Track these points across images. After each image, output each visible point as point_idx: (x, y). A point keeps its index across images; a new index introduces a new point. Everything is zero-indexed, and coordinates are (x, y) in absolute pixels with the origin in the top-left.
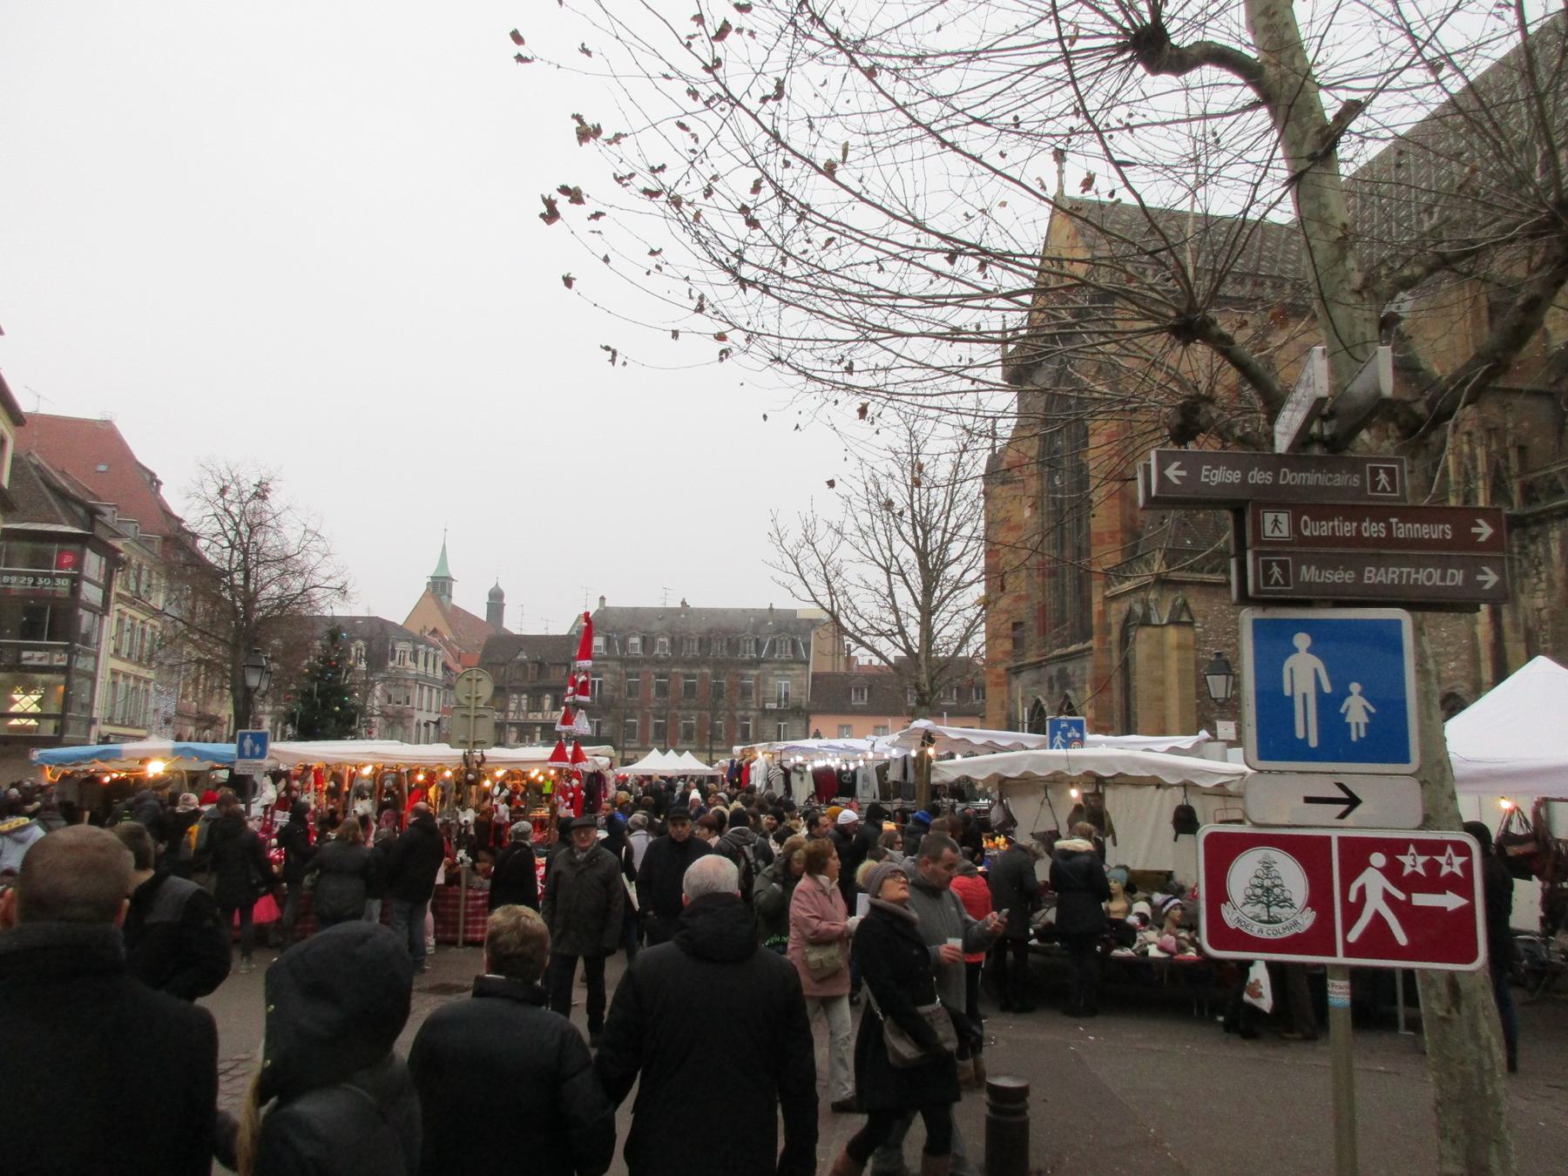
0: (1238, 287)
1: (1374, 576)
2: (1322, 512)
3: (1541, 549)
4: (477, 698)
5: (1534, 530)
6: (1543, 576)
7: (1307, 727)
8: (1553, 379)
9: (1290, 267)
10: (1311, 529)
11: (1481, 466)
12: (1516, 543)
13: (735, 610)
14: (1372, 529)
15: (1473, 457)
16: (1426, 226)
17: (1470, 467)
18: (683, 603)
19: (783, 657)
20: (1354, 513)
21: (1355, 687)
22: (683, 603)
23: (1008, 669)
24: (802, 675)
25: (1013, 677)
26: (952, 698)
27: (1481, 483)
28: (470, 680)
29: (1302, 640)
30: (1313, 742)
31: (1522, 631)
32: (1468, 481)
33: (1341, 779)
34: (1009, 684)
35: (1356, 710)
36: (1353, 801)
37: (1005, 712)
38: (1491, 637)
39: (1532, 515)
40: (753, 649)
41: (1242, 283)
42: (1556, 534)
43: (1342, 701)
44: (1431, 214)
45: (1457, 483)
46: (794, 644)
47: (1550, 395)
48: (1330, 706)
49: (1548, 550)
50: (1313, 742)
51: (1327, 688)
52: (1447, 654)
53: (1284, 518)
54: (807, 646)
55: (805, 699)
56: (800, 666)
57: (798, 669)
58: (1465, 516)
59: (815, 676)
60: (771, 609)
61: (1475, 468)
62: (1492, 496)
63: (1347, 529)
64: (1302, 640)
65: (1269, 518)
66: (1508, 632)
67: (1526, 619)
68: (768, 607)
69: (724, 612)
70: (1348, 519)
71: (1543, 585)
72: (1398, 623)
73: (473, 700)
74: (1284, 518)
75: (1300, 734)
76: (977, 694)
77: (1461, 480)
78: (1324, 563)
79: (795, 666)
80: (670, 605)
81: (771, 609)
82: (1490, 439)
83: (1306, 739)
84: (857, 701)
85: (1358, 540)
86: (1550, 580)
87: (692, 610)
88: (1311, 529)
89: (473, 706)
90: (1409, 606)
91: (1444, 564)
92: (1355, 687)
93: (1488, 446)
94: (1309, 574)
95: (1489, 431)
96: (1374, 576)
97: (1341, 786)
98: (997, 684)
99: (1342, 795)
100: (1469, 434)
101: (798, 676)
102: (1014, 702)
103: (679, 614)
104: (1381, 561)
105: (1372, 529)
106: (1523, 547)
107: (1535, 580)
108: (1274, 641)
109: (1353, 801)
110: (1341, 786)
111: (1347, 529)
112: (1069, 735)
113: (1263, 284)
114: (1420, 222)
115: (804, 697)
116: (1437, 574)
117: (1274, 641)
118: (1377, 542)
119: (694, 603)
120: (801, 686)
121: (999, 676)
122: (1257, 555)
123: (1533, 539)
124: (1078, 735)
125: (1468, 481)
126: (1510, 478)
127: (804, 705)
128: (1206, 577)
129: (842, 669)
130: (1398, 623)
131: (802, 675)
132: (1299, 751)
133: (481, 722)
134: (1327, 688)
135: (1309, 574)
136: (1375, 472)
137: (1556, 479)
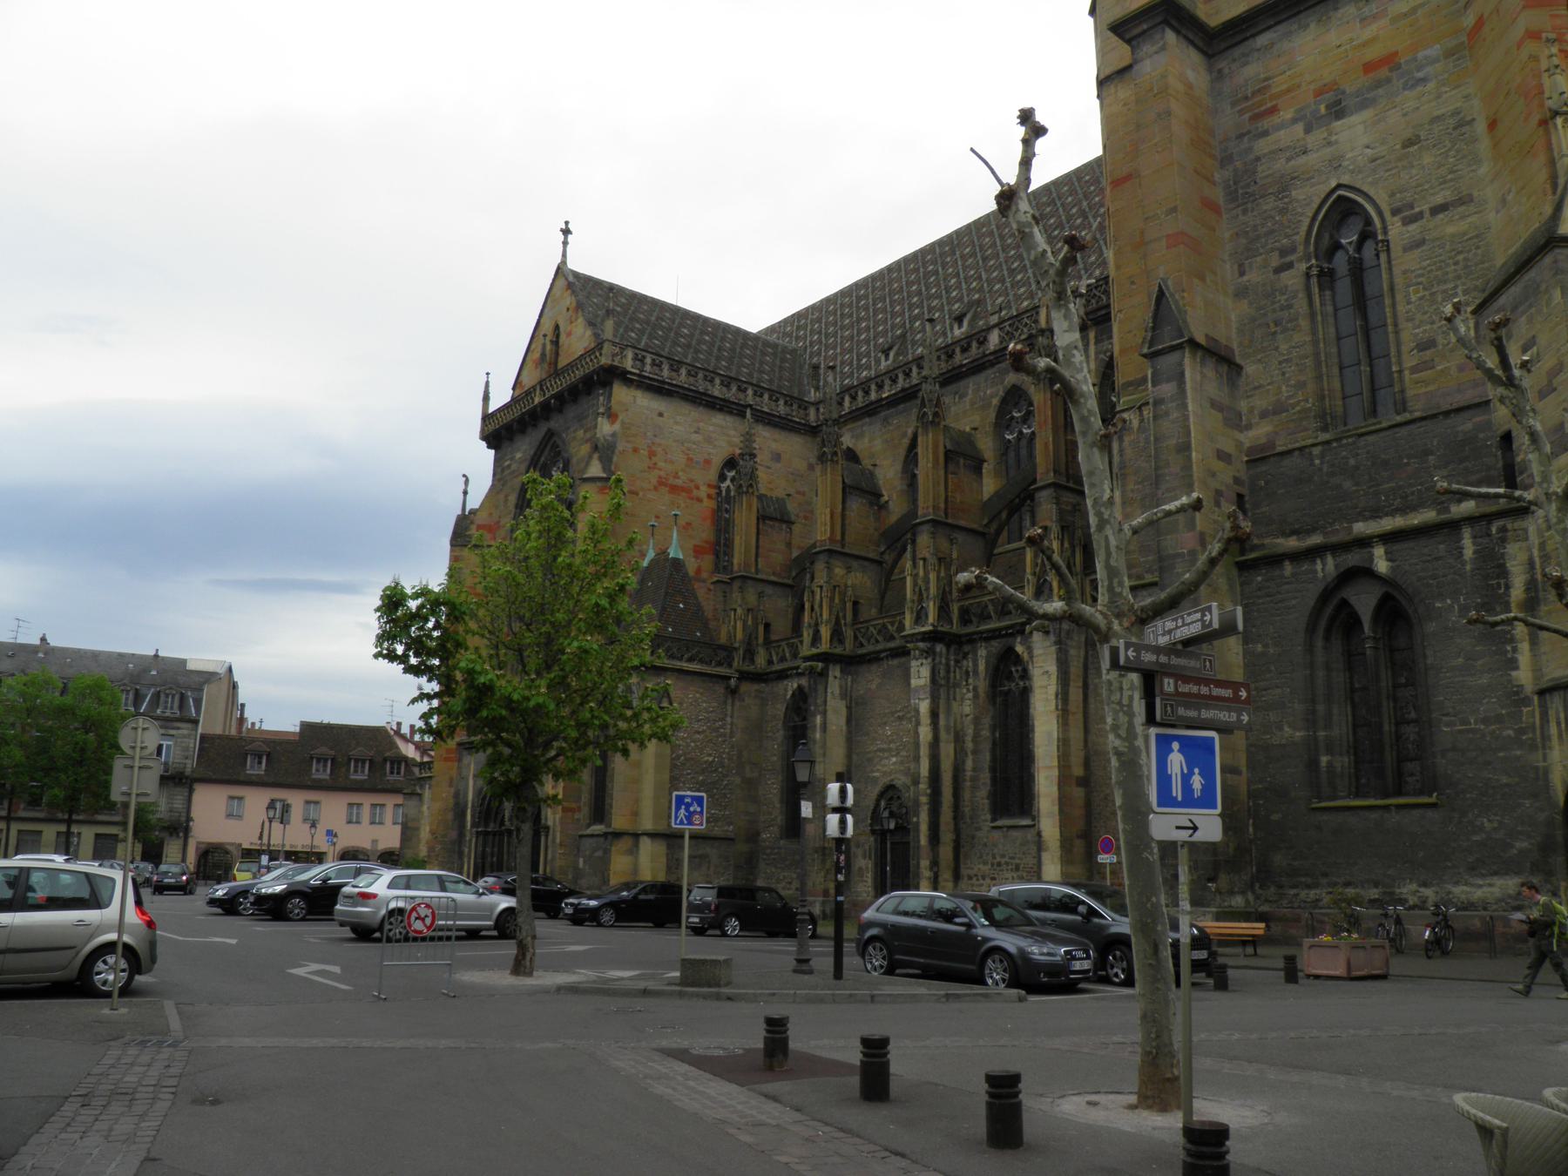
0: (724, 389)
1: (1206, 714)
2: (1187, 680)
3: (970, 664)
4: (142, 748)
5: (966, 648)
6: (971, 687)
7: (1177, 791)
8: (985, 522)
9: (637, 326)
10: (1184, 688)
11: (933, 590)
12: (952, 658)
13: (109, 655)
14: (1204, 690)
15: (927, 581)
16: (884, 365)
17: (923, 588)
18: (43, 639)
19: (168, 714)
20: (1199, 681)
21: (1196, 771)
22: (43, 639)
23: (459, 744)
24: (189, 736)
25: (465, 753)
26: (363, 772)
27: (931, 604)
28: (136, 729)
29: (1176, 746)
30: (1180, 799)
31: (952, 734)
32: (921, 600)
33: (1190, 817)
34: (460, 760)
35: (1197, 782)
36: (1195, 828)
37: (452, 790)
38: (930, 737)
39: (967, 635)
40: (130, 701)
41: (728, 386)
42: (982, 652)
43: (1191, 778)
44: (887, 356)
45: (913, 601)
46: (183, 698)
47: (983, 534)
48: (1186, 779)
49: (976, 665)
50: (1180, 799)
51: (1185, 771)
52: (890, 750)
53: (1171, 681)
54: (198, 703)
55: (190, 766)
56: (189, 725)
57: (185, 729)
58: (1235, 686)
59: (203, 737)
60: (156, 656)
61: (927, 589)
62: (939, 616)
63: (1195, 689)
64: (1176, 746)
65: (1166, 680)
66: (943, 735)
67: (955, 724)
68: (152, 653)
69: (95, 656)
70: (1196, 684)
71: (970, 695)
72: (1213, 739)
73: (138, 750)
74: (1171, 681)
75: (1174, 795)
76: (392, 768)
77: (916, 598)
78: (1187, 706)
79: (179, 725)
80: (22, 640)
81: (156, 656)
82: (940, 565)
83: (1176, 797)
84: (255, 769)
85: (1198, 696)
86: (975, 689)
87: (54, 649)
88: (1184, 688)
89: (137, 757)
90: (1218, 730)
91: (1229, 710)
92: (1196, 771)
93: (939, 572)
94: (1181, 711)
95: (940, 560)
96: (1206, 714)
97: (1190, 820)
98: (447, 759)
99: (1191, 825)
100: (924, 560)
101: (184, 736)
102: (464, 779)
103: (37, 652)
104: (1208, 707)
105: (1204, 690)
106: (957, 662)
107: (965, 691)
108: (1164, 743)
109: (1195, 828)
110: (1190, 820)
111: (1195, 689)
112: (692, 809)
113: (745, 391)
114: (878, 361)
115: (189, 762)
116: (1227, 715)
117: (1164, 743)
118: (1204, 697)
119: (53, 642)
120: (186, 749)
121: (449, 751)
122: (1162, 700)
123: (965, 656)
124: (699, 809)
125: (921, 600)
126: (952, 601)
127: (188, 771)
128: (686, 665)
129: (233, 732)
130: (1213, 739)
131: (189, 736)
132: (1173, 803)
133: (146, 773)
134: (1185, 771)
135: (1181, 711)
136: (1205, 662)
137: (987, 606)
